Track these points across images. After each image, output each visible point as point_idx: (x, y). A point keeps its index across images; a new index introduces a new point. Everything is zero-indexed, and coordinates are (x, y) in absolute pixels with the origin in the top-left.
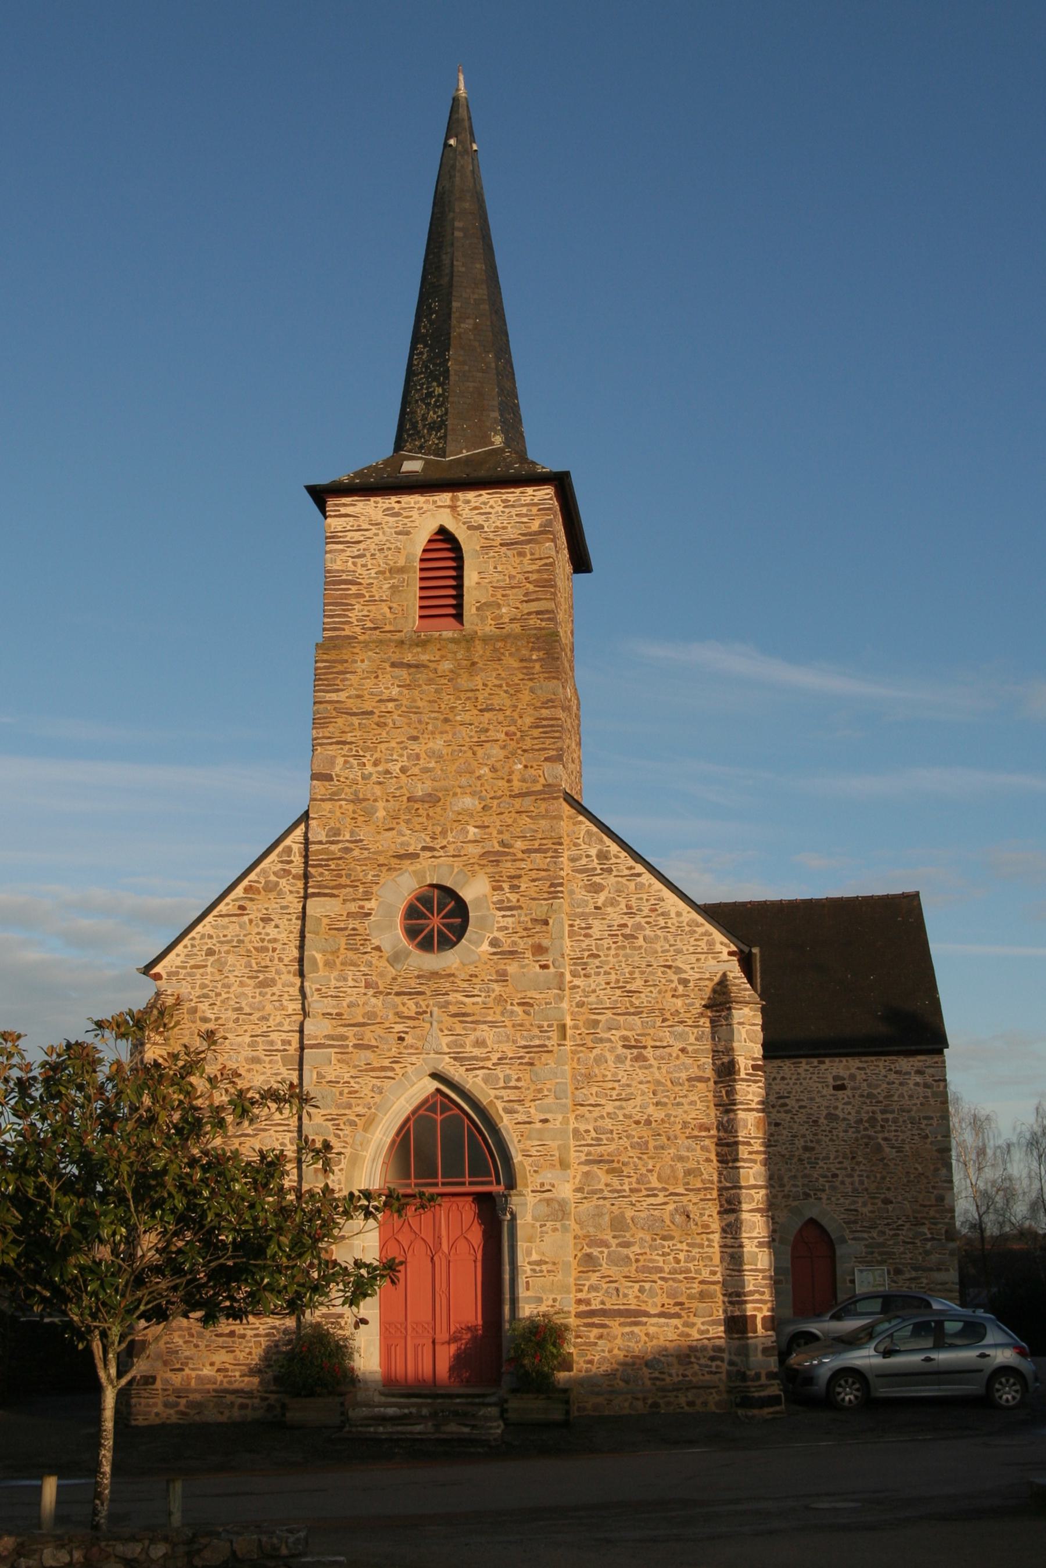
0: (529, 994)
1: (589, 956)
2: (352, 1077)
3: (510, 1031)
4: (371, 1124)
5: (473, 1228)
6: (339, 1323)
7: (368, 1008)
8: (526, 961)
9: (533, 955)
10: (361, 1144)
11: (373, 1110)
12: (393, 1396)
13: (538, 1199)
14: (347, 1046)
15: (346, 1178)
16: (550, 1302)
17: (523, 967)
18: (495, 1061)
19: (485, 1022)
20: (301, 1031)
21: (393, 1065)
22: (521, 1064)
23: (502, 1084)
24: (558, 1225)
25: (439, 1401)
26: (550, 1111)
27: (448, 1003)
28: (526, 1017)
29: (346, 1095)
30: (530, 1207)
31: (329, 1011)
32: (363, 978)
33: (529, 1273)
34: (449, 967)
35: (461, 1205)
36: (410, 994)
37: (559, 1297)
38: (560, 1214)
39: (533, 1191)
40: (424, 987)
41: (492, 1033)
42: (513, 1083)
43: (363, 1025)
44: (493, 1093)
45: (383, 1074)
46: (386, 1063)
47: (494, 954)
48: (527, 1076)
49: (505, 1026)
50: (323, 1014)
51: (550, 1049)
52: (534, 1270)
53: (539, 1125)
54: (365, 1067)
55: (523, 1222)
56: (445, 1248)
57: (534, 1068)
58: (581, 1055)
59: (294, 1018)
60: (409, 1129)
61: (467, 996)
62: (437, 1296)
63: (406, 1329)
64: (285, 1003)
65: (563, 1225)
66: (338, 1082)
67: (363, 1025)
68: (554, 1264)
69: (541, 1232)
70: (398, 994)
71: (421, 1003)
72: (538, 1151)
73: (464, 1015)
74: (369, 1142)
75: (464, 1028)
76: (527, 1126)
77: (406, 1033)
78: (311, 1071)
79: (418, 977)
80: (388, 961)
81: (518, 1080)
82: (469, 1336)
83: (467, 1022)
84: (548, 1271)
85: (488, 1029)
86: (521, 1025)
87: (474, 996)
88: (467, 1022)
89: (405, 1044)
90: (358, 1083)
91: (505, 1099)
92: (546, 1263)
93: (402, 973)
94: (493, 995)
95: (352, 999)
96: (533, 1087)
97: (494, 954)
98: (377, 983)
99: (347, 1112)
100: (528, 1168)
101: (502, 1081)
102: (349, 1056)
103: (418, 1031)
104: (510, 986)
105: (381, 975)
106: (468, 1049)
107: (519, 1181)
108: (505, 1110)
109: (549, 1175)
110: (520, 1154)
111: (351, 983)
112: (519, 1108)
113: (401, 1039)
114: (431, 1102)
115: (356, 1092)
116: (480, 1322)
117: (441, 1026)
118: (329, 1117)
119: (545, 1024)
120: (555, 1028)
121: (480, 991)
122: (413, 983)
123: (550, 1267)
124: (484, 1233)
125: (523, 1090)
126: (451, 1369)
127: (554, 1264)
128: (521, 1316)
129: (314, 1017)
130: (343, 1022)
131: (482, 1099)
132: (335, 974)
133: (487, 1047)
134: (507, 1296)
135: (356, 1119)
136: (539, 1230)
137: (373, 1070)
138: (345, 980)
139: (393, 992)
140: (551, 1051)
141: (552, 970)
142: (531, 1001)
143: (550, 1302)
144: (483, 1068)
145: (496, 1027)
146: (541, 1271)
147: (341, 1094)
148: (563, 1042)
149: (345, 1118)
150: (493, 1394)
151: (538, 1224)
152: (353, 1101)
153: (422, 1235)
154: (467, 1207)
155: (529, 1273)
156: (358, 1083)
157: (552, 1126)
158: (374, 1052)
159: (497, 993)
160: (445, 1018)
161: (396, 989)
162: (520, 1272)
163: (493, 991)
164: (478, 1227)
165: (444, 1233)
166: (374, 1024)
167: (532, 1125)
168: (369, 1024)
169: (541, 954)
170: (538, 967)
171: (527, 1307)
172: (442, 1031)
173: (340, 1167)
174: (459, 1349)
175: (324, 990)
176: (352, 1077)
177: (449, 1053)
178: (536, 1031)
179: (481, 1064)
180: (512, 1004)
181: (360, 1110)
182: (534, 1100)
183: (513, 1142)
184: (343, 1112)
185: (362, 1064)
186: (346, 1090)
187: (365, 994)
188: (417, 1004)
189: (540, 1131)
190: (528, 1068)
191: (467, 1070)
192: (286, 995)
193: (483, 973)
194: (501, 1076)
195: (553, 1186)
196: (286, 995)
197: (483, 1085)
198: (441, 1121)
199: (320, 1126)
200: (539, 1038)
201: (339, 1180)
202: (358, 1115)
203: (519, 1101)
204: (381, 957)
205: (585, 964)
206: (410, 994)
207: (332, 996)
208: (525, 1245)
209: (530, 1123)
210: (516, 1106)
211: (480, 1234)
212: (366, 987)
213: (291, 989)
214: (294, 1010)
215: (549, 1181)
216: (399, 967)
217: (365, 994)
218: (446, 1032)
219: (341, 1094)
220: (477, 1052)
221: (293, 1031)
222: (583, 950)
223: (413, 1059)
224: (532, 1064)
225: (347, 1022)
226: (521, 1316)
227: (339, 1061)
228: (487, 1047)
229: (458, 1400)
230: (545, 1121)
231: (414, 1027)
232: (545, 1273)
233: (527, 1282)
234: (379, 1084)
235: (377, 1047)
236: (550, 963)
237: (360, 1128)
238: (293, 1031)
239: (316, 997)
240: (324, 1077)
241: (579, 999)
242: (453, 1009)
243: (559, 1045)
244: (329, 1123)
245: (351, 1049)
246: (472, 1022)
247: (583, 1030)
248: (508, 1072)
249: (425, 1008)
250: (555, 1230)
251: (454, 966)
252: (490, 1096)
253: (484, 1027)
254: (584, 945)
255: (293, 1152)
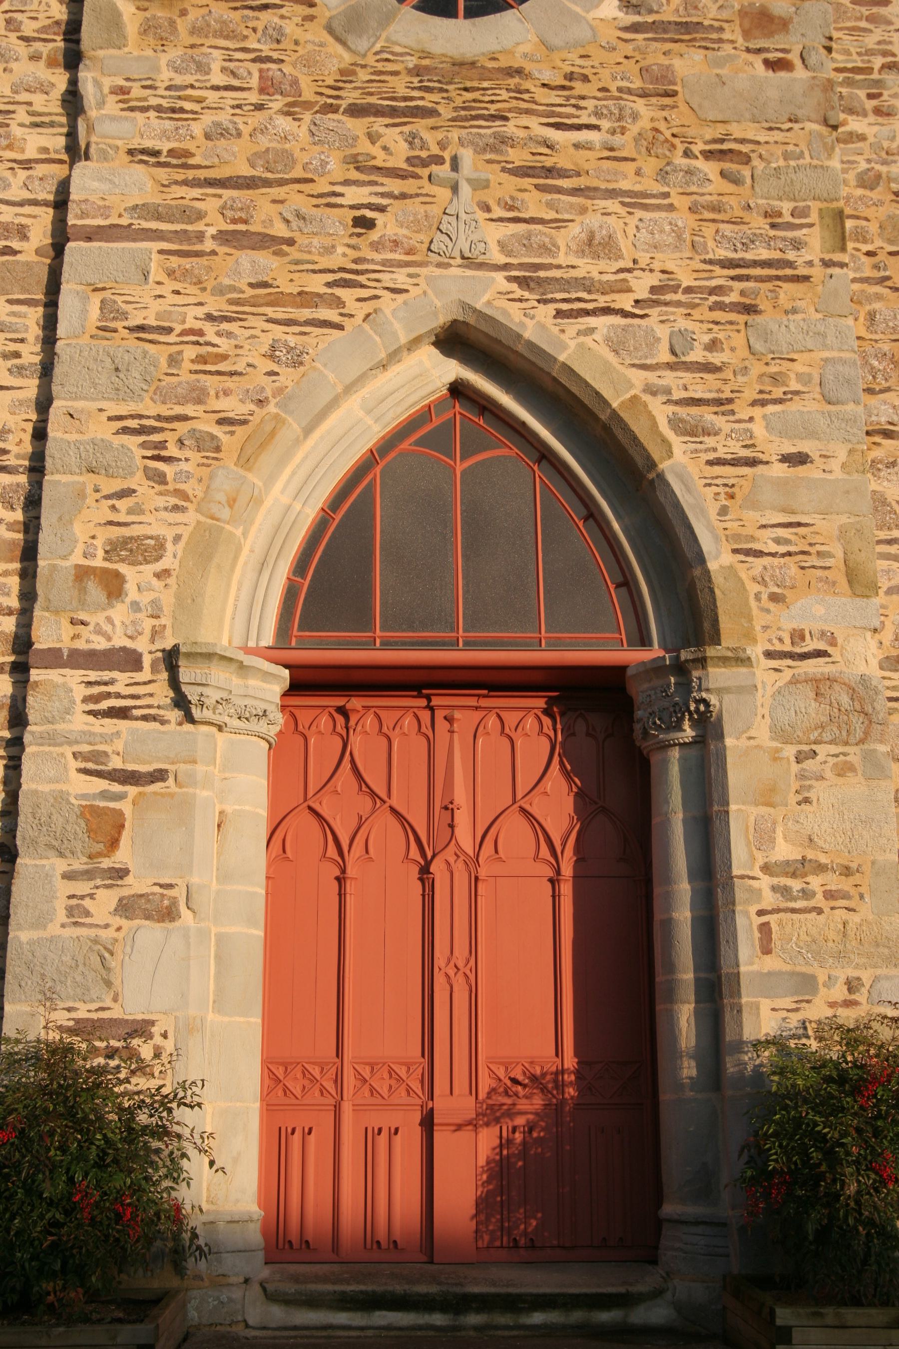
0: (737, 131)
1: (885, 67)
2: (210, 317)
3: (684, 220)
4: (263, 446)
5: (548, 784)
6: (132, 1055)
7: (264, 142)
8: (728, 48)
9: (746, 34)
10: (232, 502)
11: (272, 408)
12: (312, 1302)
13: (787, 675)
14: (200, 236)
15: (178, 596)
16: (839, 992)
17: (719, 63)
18: (644, 294)
19: (612, 194)
20: (61, 203)
21: (339, 292)
22: (719, 306)
23: (665, 356)
24: (854, 755)
25: (473, 1319)
26: (813, 434)
27: (505, 140)
28: (730, 188)
29: (187, 365)
30: (763, 698)
31: (148, 144)
32: (255, 68)
33: (769, 900)
34: (510, 52)
35: (511, 719)
36: (393, 112)
37: (866, 976)
38: (857, 722)
39: (769, 655)
40: (436, 97)
41: (633, 221)
42: (697, 355)
43: (250, 183)
44: (639, 378)
45: (306, 314)
46: (317, 284)
47: (635, 28)
48: (739, 340)
49: (671, 208)
50: (131, 152)
51: (802, 271)
52: (785, 891)
53: (779, 470)
54: (250, 292)
55: (743, 743)
56: (465, 837)
57: (758, 319)
58: (877, 306)
59: (41, 170)
60: (371, 486)
61: (557, 126)
62: (440, 981)
63: (338, 1080)
64: (17, 131)
65: (869, 757)
66: (169, 330)
67: (250, 183)
68: (847, 871)
69: (801, 776)
70: (355, 111)
71: (426, 135)
72: (778, 541)
73: (550, 172)
74: (256, 501)
75: (550, 205)
76: (745, 470)
77: (381, 209)
78: (85, 299)
79: (417, 71)
80: (330, 30)
81: (713, 346)
82: (538, 1102)
83: (559, 190)
84: (829, 895)
85: (622, 211)
86: (716, 208)
87: (579, 127)
88: (559, 190)
89: (374, 235)
90: (229, 335)
91: (677, 395)
92: (821, 868)
93: (371, 60)
94: (634, 129)
95: (223, 117)
96: (756, 368)
97: (635, 28)
98: (295, 82)
99: (189, 410)
100: (753, 588)
101: (664, 346)
102: (204, 261)
103: (414, 206)
104: (683, 107)
105: (308, 62)
106: (562, 260)
107: (725, 623)
108: (676, 424)
109: (819, 610)
110: (726, 548)
111: (218, 79)
112: (720, 422)
113: (366, 224)
114: (436, 422)
115: (224, 357)
116: (570, 1061)
117: (483, 196)
118: (133, 424)
119: (786, 207)
120: (814, 217)
121: (597, 114)
122: (399, 85)
123: (834, 882)
124: (581, 796)
125: (728, 374)
126: (483, 1205)
127: (847, 871)
128: (749, 1033)
129: (104, 157)
130: (190, 174)
131: (607, 394)
132: (174, 53)
133: (620, 257)
134: (687, 975)
135: (217, 431)
136: (795, 768)
137: (276, 301)
138: (203, 68)
139: (344, 104)
140: (806, 278)
141: (800, 73)
142: (744, 148)
143: (839, 992)
144: (607, 311)
145: (645, 207)
146: (806, 894)
147: (174, 360)
148: (838, 257)
149: (182, 428)
150: (657, 1294)
151: (790, 751)
152: (210, 382)
153: (394, 802)
154: (530, 723)
155: (769, 900)
156: (229, 335)
157: (818, 475)
158: (279, 253)
159: (644, 123)
160: (493, 174)
161: (350, 96)
162: (739, 895)
163: (635, 116)
164: (563, 784)
165: (461, 795)
166: (281, 183)
167: (760, 469)
168: (267, 183)
169: (770, 35)
170: (760, 68)
171: (765, 1004)
172: (488, 209)
173: (159, 566)
174: (504, 1143)
175: (137, 91)
176: (210, 317)
177: (506, 267)
178: (759, 224)
179: (603, 301)
180: (687, 154)
181: (232, 406)
182: (763, 403)
183: (703, 512)
184: (178, 410)
185: (243, 284)
186: (190, 352)
187: (259, 107)
188: (411, 139)
189: (781, 484)
190: (742, 318)
191: (559, 314)
192: (21, 111)
193: (605, 74)
194: (662, 332)
195: (833, 642)
196: (21, 111)
197: (611, 357)
198: (464, 473)
199: (104, 446)
200: (768, 242)
201: (154, 603)
202: (221, 422)
203: (719, 402)
204: (311, 18)
205: (878, 83)
206: (393, 112)
207: (159, 109)
208: (754, 812)
209: (752, 463)
210: (708, 415)
211: (568, 804)
212: (262, 91)
213: (39, 101)
214: (45, 150)
215: (817, 626)
216: (362, 44)
217: (259, 107)
218: (498, 212)
219: (174, 360)
220: (587, 267)
221: (35, 203)
222: (870, 52)
223: (400, 278)
224: (750, 309)
225: (202, 174)
226: (749, 1033)
227: (171, 273)
228: (620, 257)
229: (538, 1318)
230: (798, 459)
231: (403, 196)
232: (819, 900)
233: (765, 928)
234: (292, 341)
235: (291, 242)
236: (794, 57)
237: (229, 457)
238: (35, 203)
239: (112, 106)
240: (125, 316)
241: (864, 166)
242: (518, 157)
243: (827, 264)
244: (133, 442)
245: (209, 245)
246: (575, 192)
247: (879, 243)
248: (682, 324)
249: (435, 150)
250: (844, 770)
251: (522, 49)
252: (632, 386)
253: (613, 205)
254: (870, 41)
255: (11, 527)
